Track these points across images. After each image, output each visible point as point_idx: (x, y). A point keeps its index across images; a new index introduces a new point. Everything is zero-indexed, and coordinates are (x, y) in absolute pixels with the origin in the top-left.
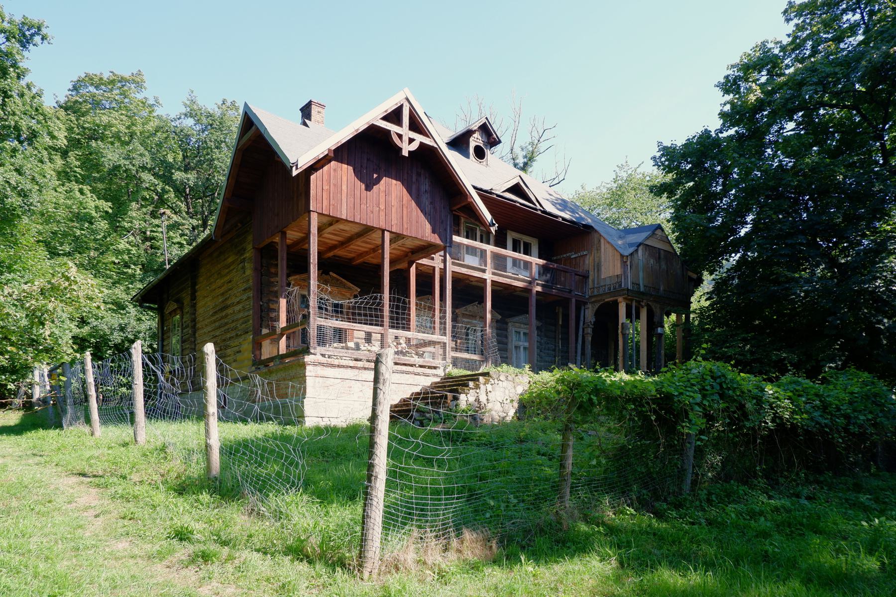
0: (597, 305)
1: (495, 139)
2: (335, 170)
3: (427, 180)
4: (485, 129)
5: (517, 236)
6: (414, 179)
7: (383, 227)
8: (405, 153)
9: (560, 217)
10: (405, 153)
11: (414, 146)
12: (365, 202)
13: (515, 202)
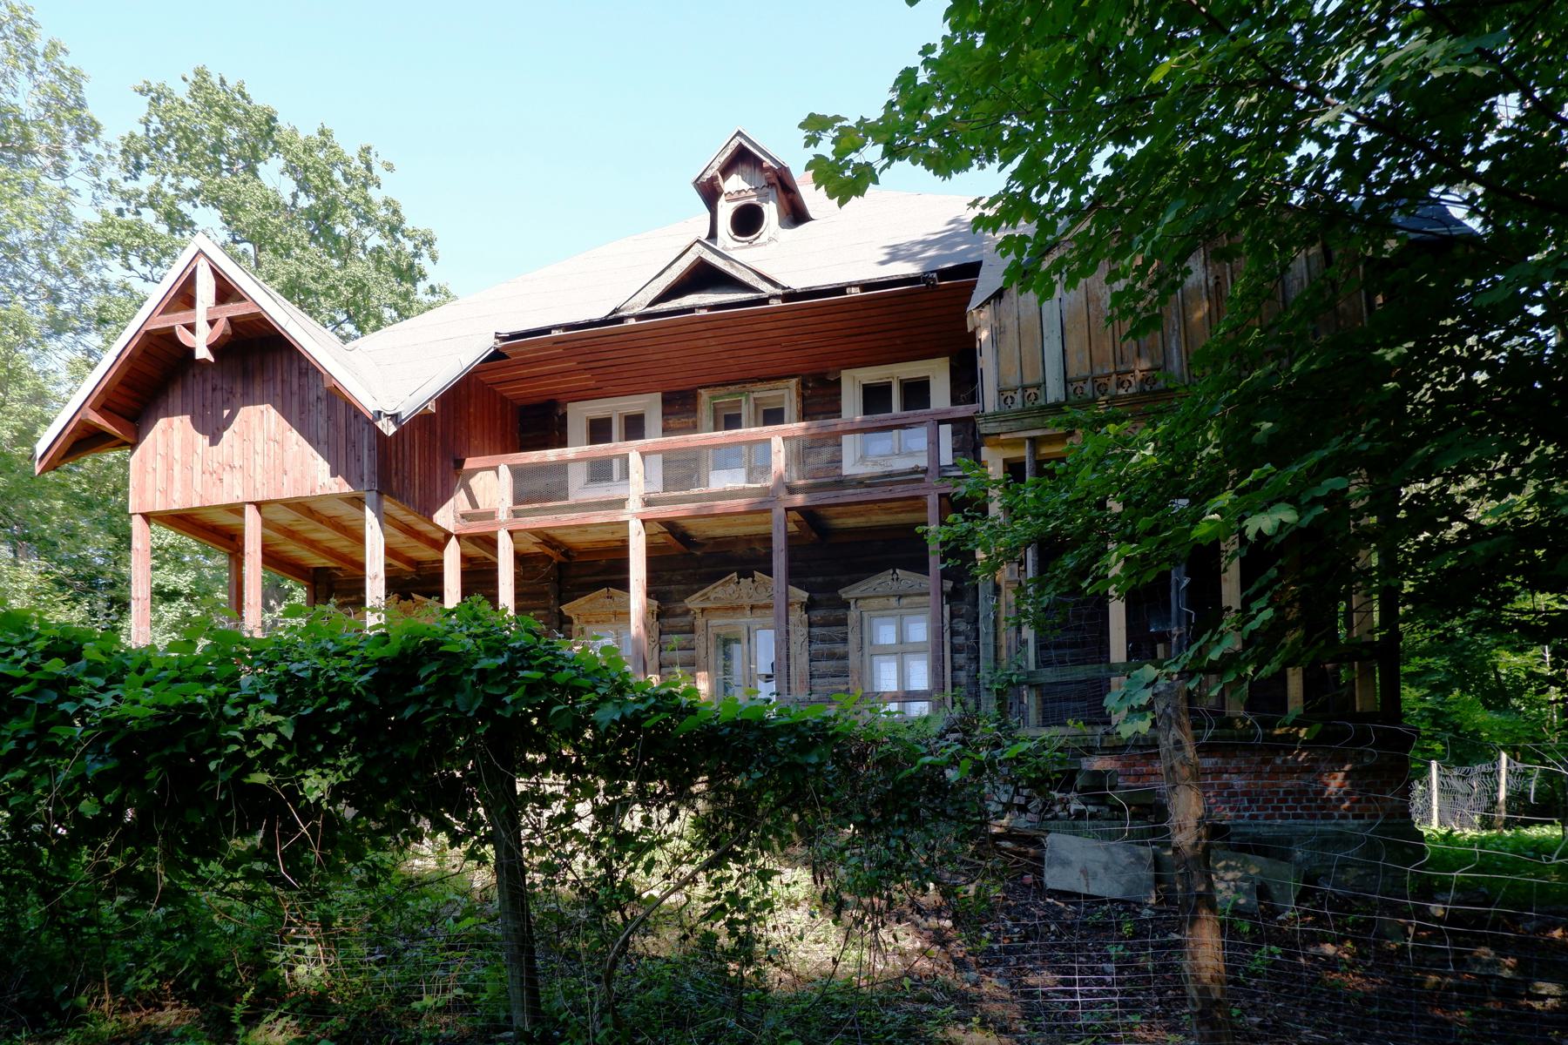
9: (851, 285)
10: (202, 353)
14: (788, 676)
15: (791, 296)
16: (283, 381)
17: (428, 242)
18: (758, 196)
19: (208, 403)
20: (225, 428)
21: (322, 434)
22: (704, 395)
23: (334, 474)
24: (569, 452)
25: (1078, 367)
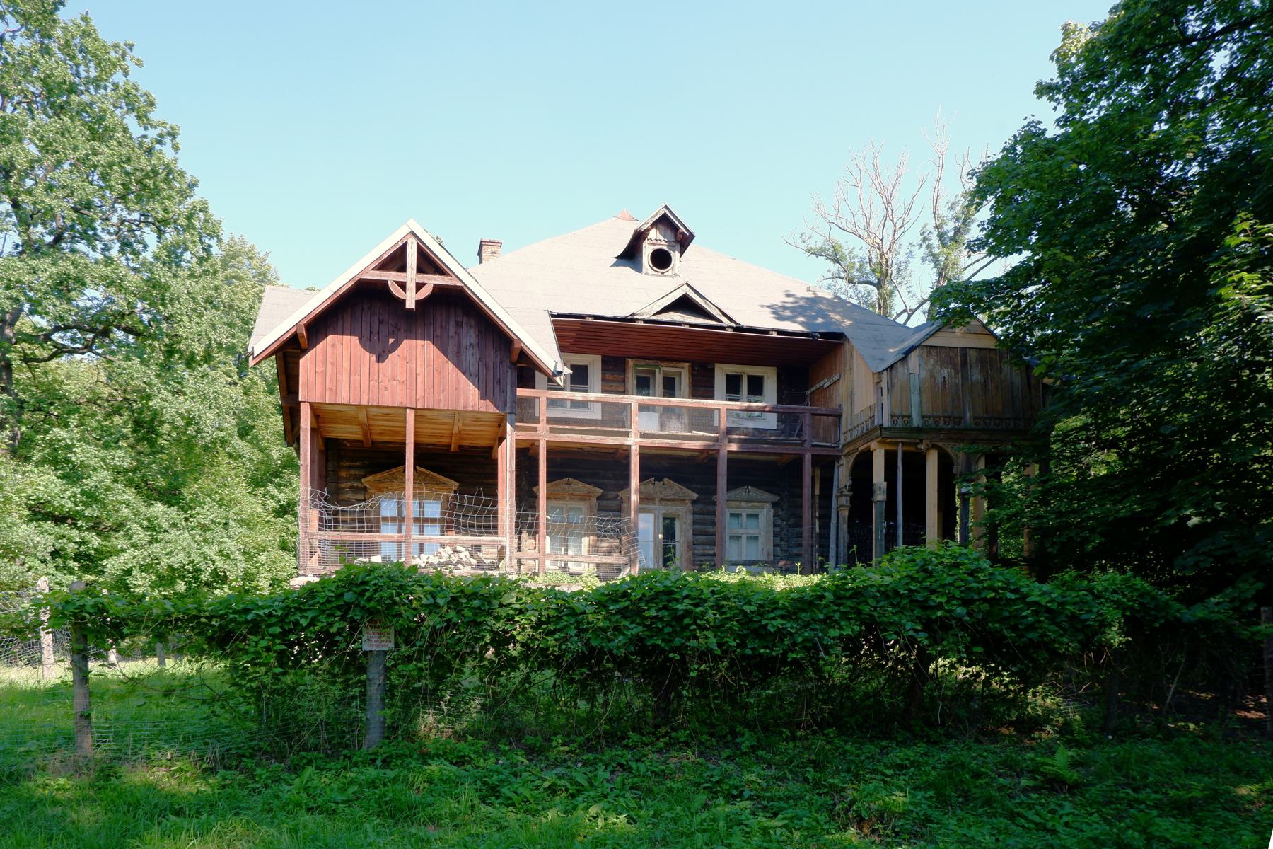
0: (852, 458)
1: (683, 234)
2: (333, 345)
3: (472, 330)
4: (665, 222)
5: (733, 369)
6: (452, 333)
7: (404, 405)
8: (410, 304)
9: (773, 330)
10: (410, 304)
11: (426, 292)
12: (376, 377)
13: (679, 324)
14: (837, 557)
15: (739, 328)
16: (441, 327)
17: (173, 135)
18: (669, 246)
19: (375, 331)
20: (390, 352)
21: (474, 369)
22: (631, 362)
23: (483, 397)
24: (591, 396)
25: (928, 410)
